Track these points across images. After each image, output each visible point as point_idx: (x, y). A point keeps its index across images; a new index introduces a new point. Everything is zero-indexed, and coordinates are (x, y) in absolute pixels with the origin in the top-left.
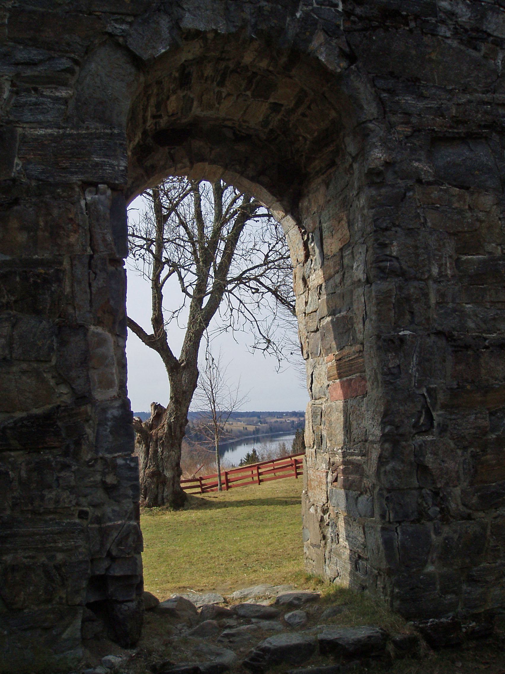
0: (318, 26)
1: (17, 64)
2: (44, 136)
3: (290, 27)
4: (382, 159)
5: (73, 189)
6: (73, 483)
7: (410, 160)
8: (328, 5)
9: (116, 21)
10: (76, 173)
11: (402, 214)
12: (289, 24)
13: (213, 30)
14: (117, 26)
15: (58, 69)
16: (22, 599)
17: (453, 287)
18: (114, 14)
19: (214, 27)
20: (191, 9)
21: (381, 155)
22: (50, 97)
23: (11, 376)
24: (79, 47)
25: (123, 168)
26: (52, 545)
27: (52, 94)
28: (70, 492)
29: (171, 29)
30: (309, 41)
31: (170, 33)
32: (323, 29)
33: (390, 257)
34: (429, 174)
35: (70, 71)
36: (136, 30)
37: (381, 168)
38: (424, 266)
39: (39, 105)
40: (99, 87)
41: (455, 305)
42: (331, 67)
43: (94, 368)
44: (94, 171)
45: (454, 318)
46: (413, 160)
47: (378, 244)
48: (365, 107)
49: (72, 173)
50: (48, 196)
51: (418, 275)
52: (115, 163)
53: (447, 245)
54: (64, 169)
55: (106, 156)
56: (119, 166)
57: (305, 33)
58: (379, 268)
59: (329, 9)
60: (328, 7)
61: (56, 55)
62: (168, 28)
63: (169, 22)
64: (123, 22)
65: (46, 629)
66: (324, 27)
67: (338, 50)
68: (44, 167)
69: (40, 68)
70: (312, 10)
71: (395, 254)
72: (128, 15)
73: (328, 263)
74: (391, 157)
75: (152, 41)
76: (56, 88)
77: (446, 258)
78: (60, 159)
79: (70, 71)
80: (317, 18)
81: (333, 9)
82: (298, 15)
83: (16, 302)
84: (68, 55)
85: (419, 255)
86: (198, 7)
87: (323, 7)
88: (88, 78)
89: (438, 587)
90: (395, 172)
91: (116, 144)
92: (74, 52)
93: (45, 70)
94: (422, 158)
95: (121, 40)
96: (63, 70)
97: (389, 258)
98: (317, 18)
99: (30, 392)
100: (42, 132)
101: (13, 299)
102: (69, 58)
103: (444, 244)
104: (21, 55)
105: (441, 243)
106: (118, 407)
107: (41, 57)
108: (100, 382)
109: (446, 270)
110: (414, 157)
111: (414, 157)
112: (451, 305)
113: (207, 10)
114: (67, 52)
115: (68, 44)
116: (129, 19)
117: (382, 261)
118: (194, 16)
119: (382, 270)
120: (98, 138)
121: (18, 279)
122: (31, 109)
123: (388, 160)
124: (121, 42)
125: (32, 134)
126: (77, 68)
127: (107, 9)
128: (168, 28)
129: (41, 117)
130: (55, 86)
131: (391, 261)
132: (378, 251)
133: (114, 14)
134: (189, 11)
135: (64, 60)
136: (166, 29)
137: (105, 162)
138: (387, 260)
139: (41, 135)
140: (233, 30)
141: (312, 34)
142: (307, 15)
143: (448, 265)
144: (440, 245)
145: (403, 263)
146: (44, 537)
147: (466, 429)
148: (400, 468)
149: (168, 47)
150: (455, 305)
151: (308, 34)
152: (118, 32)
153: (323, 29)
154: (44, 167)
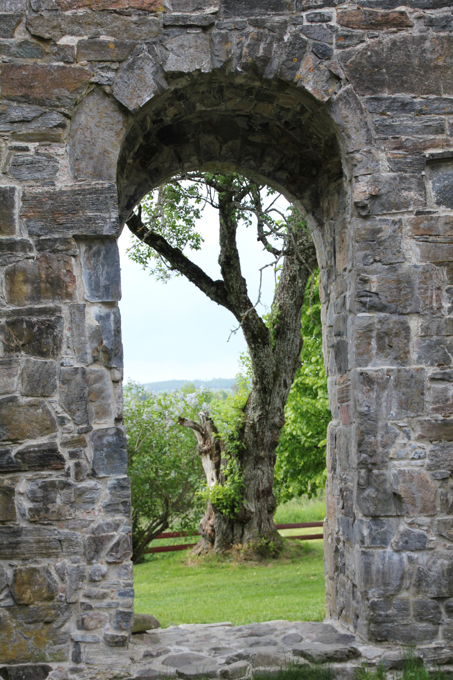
0: (307, 48)
1: (12, 122)
2: (42, 194)
3: (276, 55)
4: (367, 192)
5: (69, 243)
6: (73, 500)
7: (399, 190)
8: (320, 21)
9: (102, 69)
10: (72, 228)
11: (384, 248)
12: (275, 52)
13: (196, 70)
14: (104, 74)
15: (51, 126)
16: (28, 596)
17: (439, 319)
18: (100, 61)
19: (198, 67)
20: (174, 49)
21: (366, 188)
22: (44, 155)
23: (21, 410)
24: (69, 100)
25: (114, 220)
26: (54, 551)
27: (46, 152)
28: (71, 506)
29: (155, 73)
30: (296, 68)
31: (153, 79)
32: (312, 51)
33: (369, 294)
34: (419, 203)
35: (62, 126)
36: (121, 77)
37: (366, 202)
38: (407, 300)
39: (35, 163)
40: (89, 142)
41: (439, 338)
42: (317, 97)
43: (91, 401)
44: (88, 225)
45: (438, 351)
46: (403, 189)
47: (360, 280)
48: (353, 136)
49: (68, 228)
50: (48, 250)
51: (400, 309)
52: (107, 215)
53: (434, 276)
54: (61, 224)
55: (98, 210)
56: (110, 218)
57: (292, 60)
58: (361, 302)
59: (320, 25)
60: (319, 24)
61: (47, 110)
62: (152, 74)
63: (153, 66)
64: (109, 69)
65: (47, 623)
66: (314, 49)
67: (327, 73)
68: (43, 223)
69: (34, 125)
70: (301, 30)
71: (374, 290)
72: (113, 62)
73: (125, 425)
74: (377, 189)
75: (137, 89)
76: (49, 145)
77: (432, 290)
78: (57, 216)
79: (62, 126)
80: (306, 38)
81: (324, 25)
82: (286, 38)
83: (23, 345)
84: (59, 109)
85: (401, 290)
86: (181, 45)
87: (313, 24)
88: (79, 133)
89: (412, 613)
90: (382, 205)
91: (106, 197)
92: (64, 106)
93: (39, 127)
94: (413, 186)
95: (108, 89)
96: (55, 127)
97: (369, 294)
98: (306, 38)
99: (36, 422)
100: (40, 190)
101: (21, 343)
102: (62, 113)
103: (431, 276)
104: (16, 114)
105: (428, 275)
106: (113, 435)
107: (34, 115)
108: (97, 413)
109: (431, 303)
110: (403, 186)
111: (403, 186)
112: (435, 338)
113: (190, 48)
114: (57, 106)
115: (59, 99)
116: (115, 66)
117: (362, 296)
118: (178, 56)
119: (364, 304)
120: (90, 194)
121: (25, 326)
122: (28, 168)
123: (373, 194)
124: (107, 92)
125: (31, 193)
126: (68, 122)
127: (92, 57)
128: (152, 74)
129: (38, 175)
130: (48, 143)
131: (370, 296)
132: (360, 286)
133: (100, 61)
134: (172, 50)
135: (55, 116)
136: (149, 75)
137: (97, 216)
138: (367, 296)
139: (39, 193)
140: (218, 65)
141: (300, 59)
142: (296, 36)
143: (434, 297)
144: (426, 278)
145: (383, 298)
146: (48, 545)
147: (446, 461)
148: (374, 496)
149: (153, 95)
150: (439, 338)
151: (296, 60)
152: (104, 81)
153: (312, 51)
154: (43, 223)
